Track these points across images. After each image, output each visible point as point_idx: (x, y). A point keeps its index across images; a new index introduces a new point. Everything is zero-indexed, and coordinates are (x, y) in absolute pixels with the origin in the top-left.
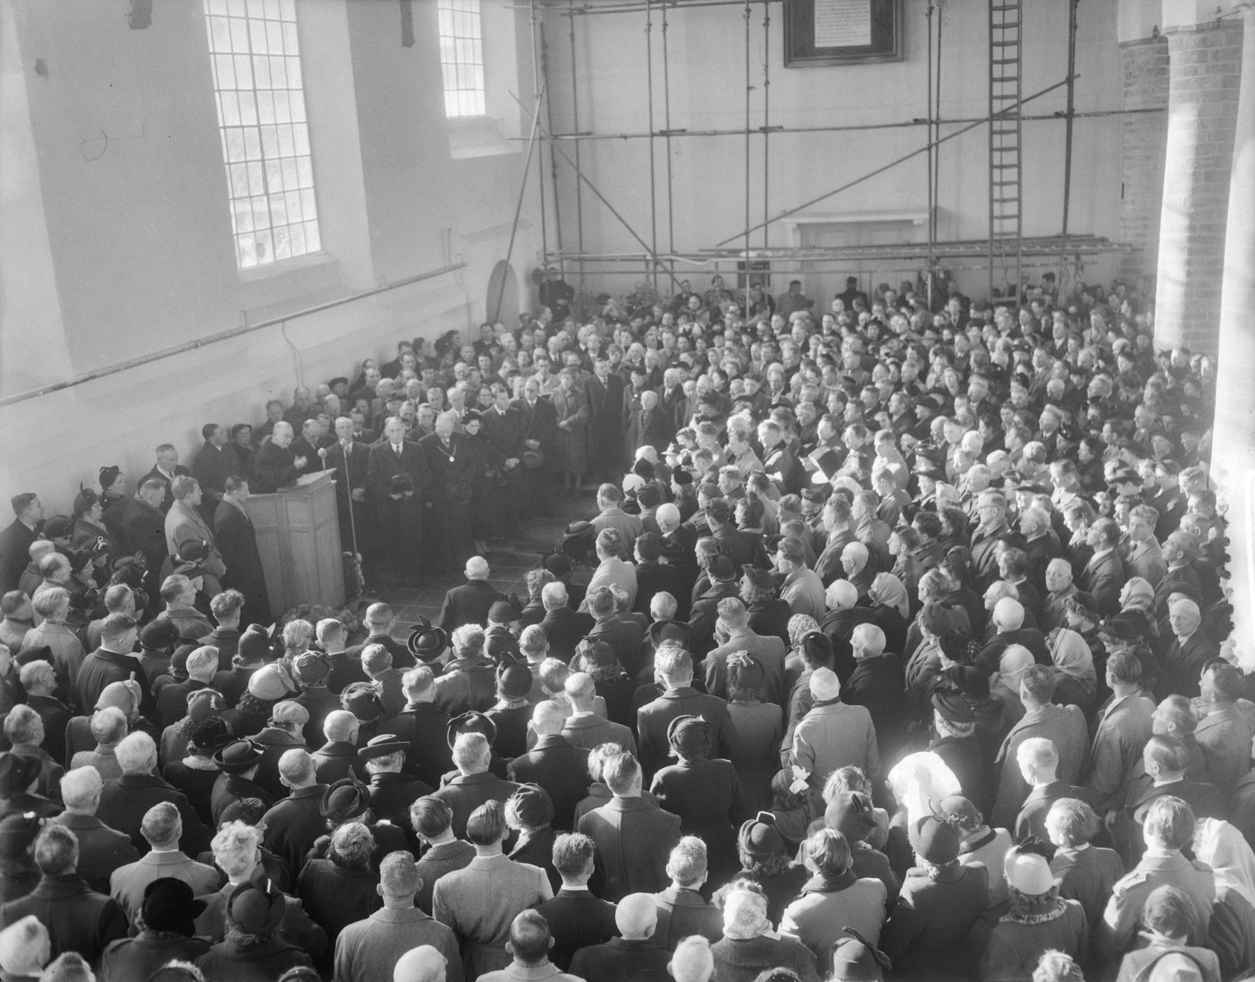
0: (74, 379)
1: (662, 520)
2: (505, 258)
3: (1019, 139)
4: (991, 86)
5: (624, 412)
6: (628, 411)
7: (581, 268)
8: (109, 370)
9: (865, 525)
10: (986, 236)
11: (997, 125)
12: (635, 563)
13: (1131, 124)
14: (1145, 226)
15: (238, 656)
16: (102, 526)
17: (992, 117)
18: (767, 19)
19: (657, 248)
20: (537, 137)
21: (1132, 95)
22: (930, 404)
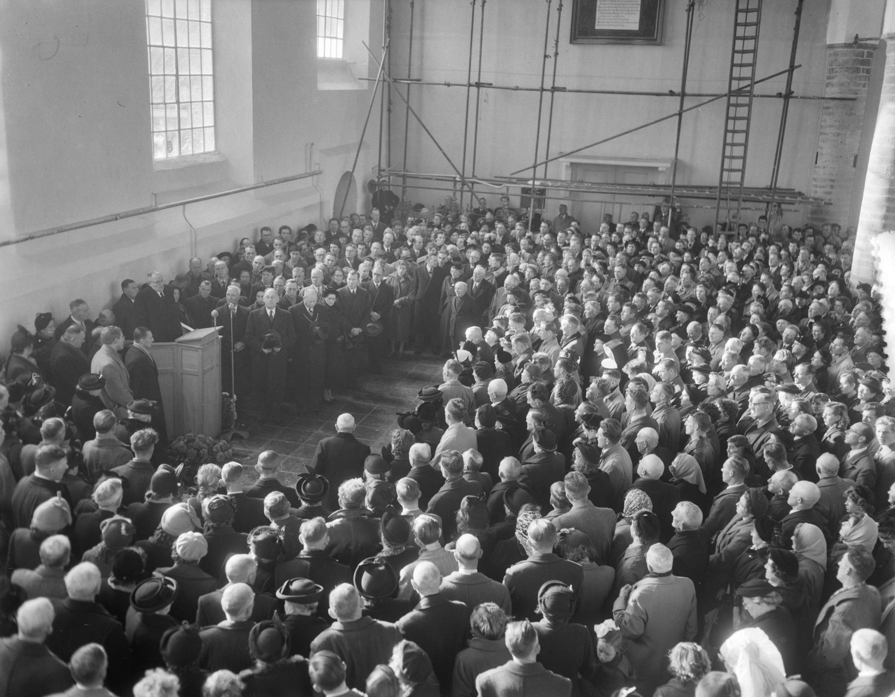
0: (17, 238)
1: (493, 392)
2: (351, 170)
3: (750, 111)
5: (442, 297)
6: (445, 297)
8: (46, 233)
9: (660, 409)
10: (716, 183)
11: (733, 100)
12: (476, 428)
13: (828, 108)
14: (832, 187)
15: (150, 492)
16: (33, 361)
17: (731, 93)
18: (561, 5)
19: (465, 172)
20: (382, 79)
21: (832, 86)
22: (687, 310)
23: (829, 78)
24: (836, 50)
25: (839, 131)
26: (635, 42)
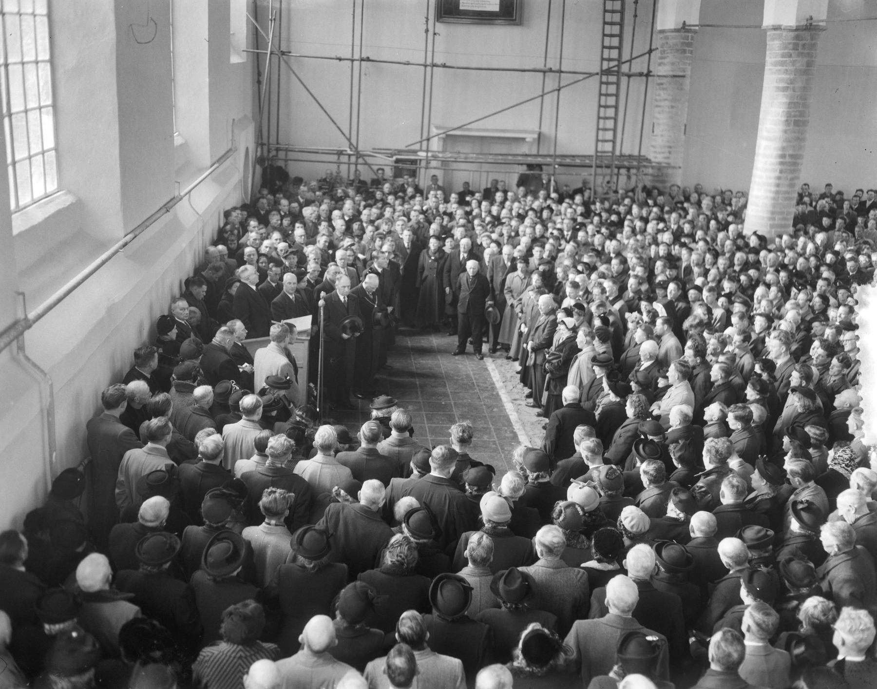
7: (286, 155)
10: (592, 152)
11: (604, 79)
14: (670, 153)
21: (665, 64)
23: (661, 58)
24: (666, 34)
25: (673, 104)
26: (497, 22)
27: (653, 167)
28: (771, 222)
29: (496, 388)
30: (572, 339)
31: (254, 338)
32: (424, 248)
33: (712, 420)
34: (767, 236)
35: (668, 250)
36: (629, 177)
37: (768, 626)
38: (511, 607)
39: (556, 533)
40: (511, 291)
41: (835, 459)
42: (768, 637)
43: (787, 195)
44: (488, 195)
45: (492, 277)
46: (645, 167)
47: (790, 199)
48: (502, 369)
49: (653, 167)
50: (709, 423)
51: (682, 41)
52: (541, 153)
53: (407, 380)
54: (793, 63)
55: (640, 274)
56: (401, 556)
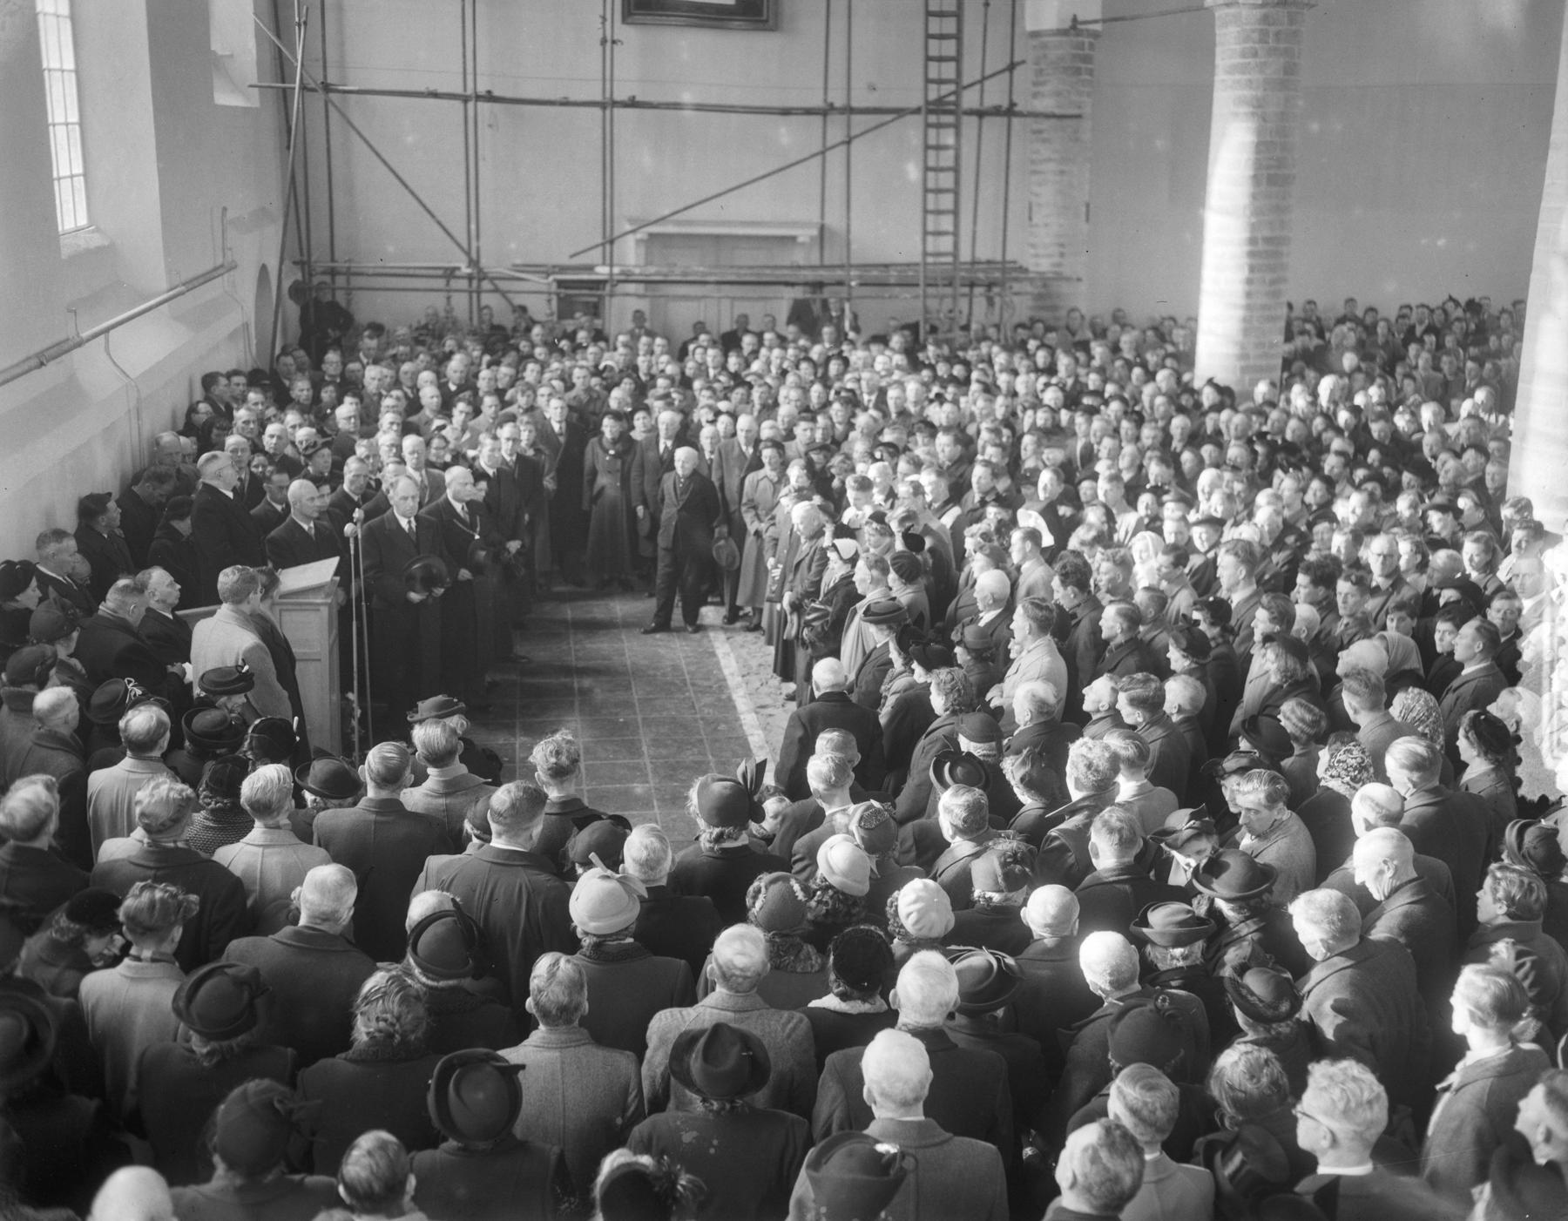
4: (926, 67)
7: (348, 282)
10: (918, 258)
11: (932, 119)
21: (1043, 95)
23: (1035, 84)
27: (1031, 280)
28: (1243, 363)
29: (727, 687)
30: (847, 580)
31: (206, 605)
32: (595, 435)
33: (1098, 711)
34: (1235, 388)
35: (1054, 418)
36: (990, 302)
37: (1153, 1112)
38: (723, 1108)
39: (750, 948)
40: (755, 508)
41: (1331, 767)
42: (1161, 1138)
43: (1267, 313)
44: (729, 342)
45: (722, 479)
46: (1016, 280)
47: (1272, 319)
48: (744, 652)
49: (1031, 280)
50: (1095, 717)
51: (1074, 52)
52: (827, 262)
53: (553, 681)
54: (1262, 67)
55: (994, 460)
56: (385, 1020)
